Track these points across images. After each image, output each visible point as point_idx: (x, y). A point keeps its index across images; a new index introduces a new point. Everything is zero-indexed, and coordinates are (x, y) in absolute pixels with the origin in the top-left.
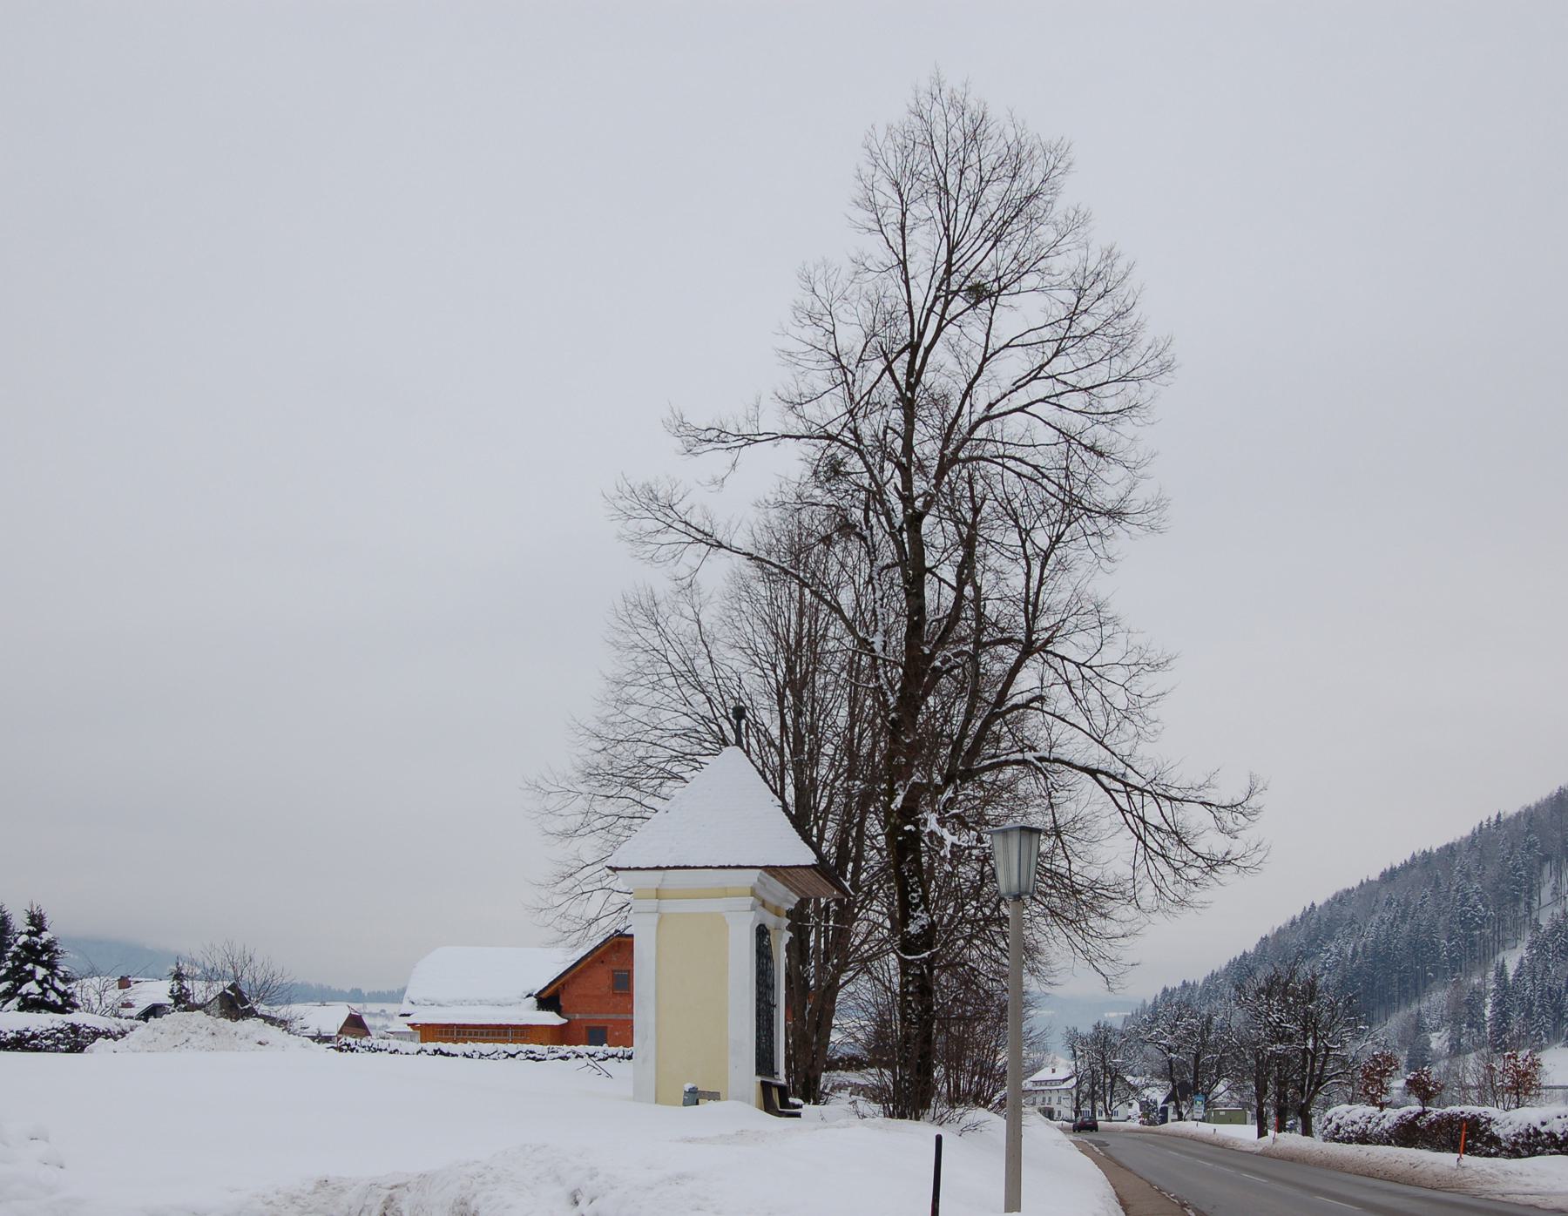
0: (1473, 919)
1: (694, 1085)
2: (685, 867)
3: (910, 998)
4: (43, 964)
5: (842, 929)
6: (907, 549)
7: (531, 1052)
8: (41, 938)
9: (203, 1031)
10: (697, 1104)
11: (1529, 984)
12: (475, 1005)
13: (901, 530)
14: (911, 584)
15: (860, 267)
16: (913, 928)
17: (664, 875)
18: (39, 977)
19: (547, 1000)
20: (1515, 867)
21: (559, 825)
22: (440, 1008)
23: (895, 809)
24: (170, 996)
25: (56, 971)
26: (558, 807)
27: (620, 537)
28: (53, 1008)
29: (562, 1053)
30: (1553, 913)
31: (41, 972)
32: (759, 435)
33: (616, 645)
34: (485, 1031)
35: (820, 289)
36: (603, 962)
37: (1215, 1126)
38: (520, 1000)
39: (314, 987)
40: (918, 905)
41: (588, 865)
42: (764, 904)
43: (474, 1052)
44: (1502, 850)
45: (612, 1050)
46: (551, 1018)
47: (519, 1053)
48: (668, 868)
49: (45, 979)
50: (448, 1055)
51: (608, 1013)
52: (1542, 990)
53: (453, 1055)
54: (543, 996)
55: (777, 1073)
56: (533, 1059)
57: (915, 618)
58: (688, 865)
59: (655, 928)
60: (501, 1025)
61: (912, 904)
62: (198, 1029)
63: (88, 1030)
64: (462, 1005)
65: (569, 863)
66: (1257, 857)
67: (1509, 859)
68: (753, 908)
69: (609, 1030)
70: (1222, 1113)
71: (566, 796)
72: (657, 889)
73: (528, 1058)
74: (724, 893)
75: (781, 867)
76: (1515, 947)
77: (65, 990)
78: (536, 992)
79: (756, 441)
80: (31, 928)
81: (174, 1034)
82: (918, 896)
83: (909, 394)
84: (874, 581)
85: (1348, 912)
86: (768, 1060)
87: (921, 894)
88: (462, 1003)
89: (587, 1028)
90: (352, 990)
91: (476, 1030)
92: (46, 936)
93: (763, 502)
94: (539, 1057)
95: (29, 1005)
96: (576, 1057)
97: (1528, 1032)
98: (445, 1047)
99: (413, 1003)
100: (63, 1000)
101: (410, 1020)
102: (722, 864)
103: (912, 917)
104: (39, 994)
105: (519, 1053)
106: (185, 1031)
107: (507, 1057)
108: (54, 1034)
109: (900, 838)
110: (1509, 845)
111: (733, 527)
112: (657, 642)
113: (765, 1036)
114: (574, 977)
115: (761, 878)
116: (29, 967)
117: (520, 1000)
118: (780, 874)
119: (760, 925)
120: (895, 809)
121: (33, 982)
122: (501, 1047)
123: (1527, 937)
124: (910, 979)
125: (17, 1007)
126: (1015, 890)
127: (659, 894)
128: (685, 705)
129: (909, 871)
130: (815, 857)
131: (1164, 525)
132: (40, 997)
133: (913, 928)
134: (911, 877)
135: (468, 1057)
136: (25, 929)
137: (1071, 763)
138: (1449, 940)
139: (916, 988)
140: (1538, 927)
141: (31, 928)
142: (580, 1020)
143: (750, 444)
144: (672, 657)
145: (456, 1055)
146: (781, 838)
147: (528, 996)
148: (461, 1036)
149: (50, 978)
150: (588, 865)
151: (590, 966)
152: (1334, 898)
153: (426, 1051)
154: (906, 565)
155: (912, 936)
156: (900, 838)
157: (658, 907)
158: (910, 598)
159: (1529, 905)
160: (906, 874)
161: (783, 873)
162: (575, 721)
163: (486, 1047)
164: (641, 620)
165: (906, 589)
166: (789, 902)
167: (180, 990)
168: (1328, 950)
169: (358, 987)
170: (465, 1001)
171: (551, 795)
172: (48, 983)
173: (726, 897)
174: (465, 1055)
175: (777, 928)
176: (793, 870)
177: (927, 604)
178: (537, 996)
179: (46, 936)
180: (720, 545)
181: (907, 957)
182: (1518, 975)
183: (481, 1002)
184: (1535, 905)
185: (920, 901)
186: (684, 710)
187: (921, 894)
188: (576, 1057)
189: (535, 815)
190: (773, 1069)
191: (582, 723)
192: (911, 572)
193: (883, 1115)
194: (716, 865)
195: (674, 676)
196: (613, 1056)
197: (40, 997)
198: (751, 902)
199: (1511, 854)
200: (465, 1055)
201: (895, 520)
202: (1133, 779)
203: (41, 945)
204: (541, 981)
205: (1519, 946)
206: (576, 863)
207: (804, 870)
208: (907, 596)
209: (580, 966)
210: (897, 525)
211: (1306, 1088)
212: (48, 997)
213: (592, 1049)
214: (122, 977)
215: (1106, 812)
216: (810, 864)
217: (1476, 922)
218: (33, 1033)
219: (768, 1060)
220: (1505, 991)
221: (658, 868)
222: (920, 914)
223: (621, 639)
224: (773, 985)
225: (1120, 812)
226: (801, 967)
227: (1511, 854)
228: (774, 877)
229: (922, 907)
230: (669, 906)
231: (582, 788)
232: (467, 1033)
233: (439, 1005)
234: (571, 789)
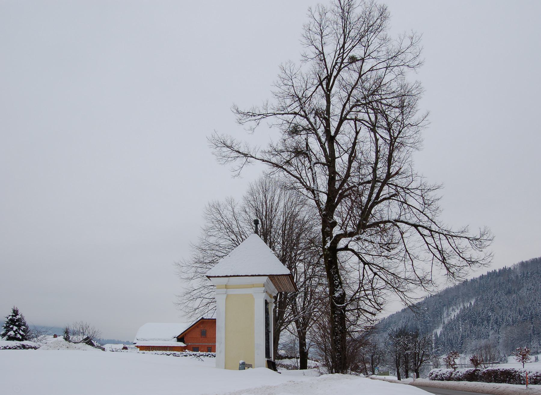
0: (427, 321)
2: (238, 276)
3: (336, 323)
4: (16, 326)
5: (281, 311)
7: (175, 354)
8: (16, 317)
9: (64, 346)
10: (245, 369)
11: (443, 338)
12: (157, 340)
14: (330, 163)
15: (305, 58)
17: (229, 279)
18: (14, 329)
19: (180, 339)
20: (436, 308)
21: (186, 276)
23: (327, 248)
24: (63, 338)
25: (21, 328)
28: (18, 339)
29: (185, 354)
30: (448, 320)
31: (15, 328)
32: (268, 114)
34: (160, 348)
35: (287, 72)
36: (198, 327)
37: (385, 376)
38: (171, 339)
39: (116, 340)
40: (338, 286)
41: (195, 290)
44: (433, 304)
45: (202, 353)
46: (181, 344)
47: (171, 354)
48: (231, 276)
49: (16, 330)
51: (199, 343)
52: (447, 339)
54: (179, 337)
55: (271, 358)
57: (332, 175)
58: (239, 275)
62: (63, 346)
63: (28, 347)
65: (189, 289)
66: (489, 260)
67: (435, 306)
69: (200, 348)
70: (382, 372)
72: (226, 285)
74: (253, 286)
75: (276, 275)
76: (438, 328)
77: (23, 334)
79: (267, 116)
80: (13, 314)
81: (54, 347)
82: (338, 282)
83: (328, 93)
85: (393, 320)
88: (153, 340)
89: (192, 347)
90: (127, 341)
92: (18, 317)
95: (10, 338)
96: (190, 356)
97: (444, 350)
99: (138, 340)
100: (22, 337)
101: (136, 345)
103: (336, 290)
104: (14, 335)
105: (171, 354)
106: (58, 346)
108: (17, 348)
109: (329, 259)
110: (434, 302)
114: (189, 332)
115: (268, 280)
116: (11, 326)
117: (171, 339)
120: (327, 248)
121: (12, 331)
123: (442, 325)
125: (6, 339)
127: (226, 287)
131: (421, 147)
132: (14, 336)
133: (337, 295)
134: (335, 274)
136: (11, 314)
137: (408, 223)
138: (421, 327)
139: (339, 319)
140: (444, 323)
141: (13, 314)
142: (191, 345)
143: (264, 118)
147: (174, 338)
149: (18, 330)
150: (195, 290)
151: (193, 329)
152: (390, 316)
156: (329, 259)
158: (330, 168)
159: (441, 317)
160: (333, 273)
162: (192, 243)
167: (67, 336)
168: (389, 330)
169: (128, 340)
172: (17, 331)
173: (254, 287)
178: (177, 338)
179: (18, 317)
181: (338, 305)
182: (440, 335)
184: (442, 317)
188: (190, 356)
192: (330, 158)
194: (250, 275)
196: (202, 355)
197: (14, 336)
199: (435, 304)
202: (434, 228)
203: (16, 320)
204: (178, 333)
205: (439, 328)
206: (191, 289)
209: (190, 329)
211: (417, 364)
212: (17, 336)
213: (195, 353)
214: (55, 335)
215: (418, 245)
216: (288, 274)
217: (428, 322)
218: (9, 347)
220: (437, 339)
221: (227, 276)
222: (339, 289)
225: (426, 244)
227: (435, 304)
229: (340, 286)
230: (231, 291)
233: (146, 340)
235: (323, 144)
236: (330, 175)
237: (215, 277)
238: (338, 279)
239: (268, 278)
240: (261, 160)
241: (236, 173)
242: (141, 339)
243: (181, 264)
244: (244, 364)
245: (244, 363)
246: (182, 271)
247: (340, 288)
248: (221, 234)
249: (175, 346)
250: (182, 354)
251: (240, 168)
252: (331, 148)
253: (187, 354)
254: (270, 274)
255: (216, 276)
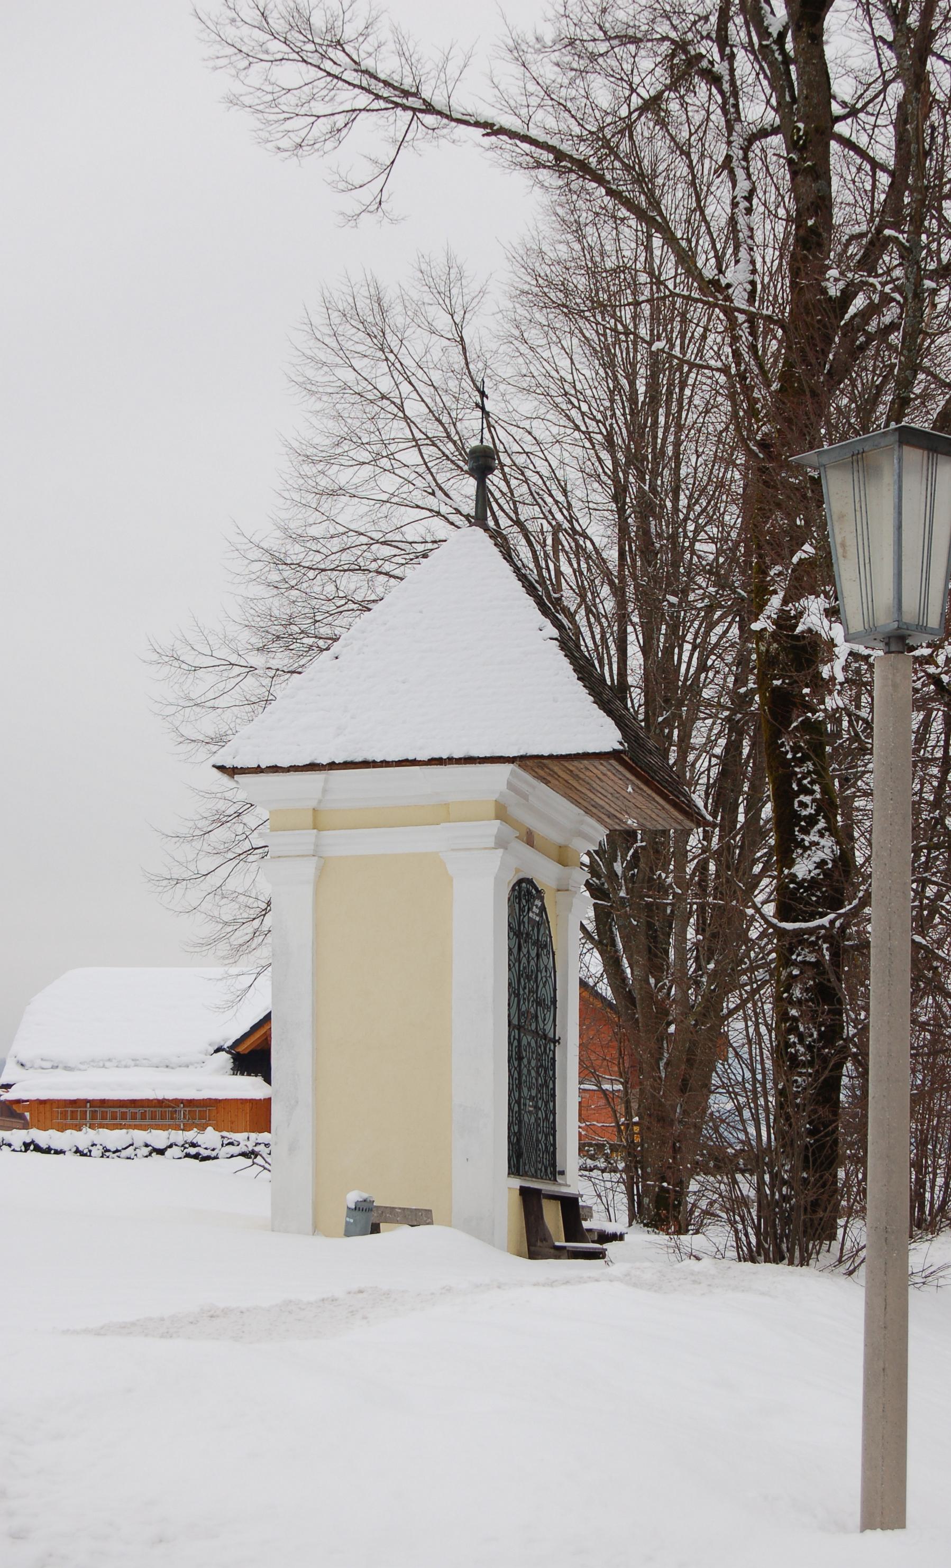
1: (365, 1195)
2: (366, 764)
6: (794, 77)
7: (194, 1145)
13: (782, 36)
14: (802, 150)
16: (803, 868)
17: (326, 781)
22: (66, 1072)
26: (211, 695)
27: (233, 101)
33: (309, 388)
38: (203, 1057)
42: (529, 839)
43: (93, 1145)
47: (170, 1146)
48: (332, 766)
50: (48, 1151)
53: (57, 1152)
54: (241, 1049)
55: (562, 1173)
56: (196, 1156)
58: (370, 758)
59: (309, 890)
60: (193, 1100)
61: (800, 818)
64: (104, 1066)
68: (501, 843)
71: (225, 674)
73: (188, 1155)
75: (551, 757)
78: (229, 1043)
82: (813, 801)
84: (734, 164)
86: (542, 1146)
87: (818, 796)
88: (102, 1063)
91: (124, 1110)
93: (532, 40)
94: (205, 1153)
98: (43, 1137)
102: (436, 756)
103: (800, 844)
105: (170, 1146)
107: (150, 1154)
109: (777, 683)
111: (452, 69)
112: (385, 385)
113: (532, 1098)
117: (203, 1057)
118: (554, 774)
119: (520, 882)
122: (140, 1136)
124: (796, 972)
126: (885, 621)
128: (433, 494)
129: (796, 749)
130: (618, 735)
133: (803, 868)
134: (800, 762)
135: (83, 1154)
139: (807, 990)
144: (414, 408)
145: (61, 1152)
146: (555, 700)
148: (98, 1121)
153: (10, 1145)
154: (792, 113)
155: (800, 884)
156: (777, 683)
157: (317, 845)
158: (800, 178)
160: (789, 756)
161: (556, 769)
163: (114, 1137)
164: (356, 341)
165: (790, 162)
166: (588, 838)
170: (110, 1060)
171: (200, 673)
174: (77, 1151)
175: (562, 889)
176: (576, 763)
177: (834, 195)
180: (429, 109)
183: (136, 1063)
185: (818, 811)
186: (432, 502)
187: (818, 796)
189: (172, 709)
190: (554, 1165)
191: (256, 539)
192: (801, 125)
193: (734, 1254)
194: (425, 758)
195: (417, 445)
198: (495, 831)
200: (77, 1151)
201: (769, 20)
207: (597, 763)
208: (794, 174)
210: (774, 31)
216: (608, 749)
219: (542, 1146)
221: (312, 767)
222: (816, 839)
223: (320, 376)
224: (554, 1001)
226: (652, 981)
228: (547, 783)
229: (822, 824)
231: (257, 660)
232: (138, 1116)
233: (66, 1068)
234: (233, 659)
235: (774, 42)
236: (797, 219)
237: (258, 770)
238: (817, 788)
239: (512, 773)
240: (477, 124)
241: (367, 195)
242: (38, 1063)
243: (190, 658)
244: (370, 1210)
245: (365, 1206)
246: (193, 696)
247: (819, 831)
248: (389, 483)
249: (217, 1101)
250: (231, 1144)
251: (377, 171)
252: (805, 63)
253: (257, 1144)
254: (522, 753)
255: (263, 766)
